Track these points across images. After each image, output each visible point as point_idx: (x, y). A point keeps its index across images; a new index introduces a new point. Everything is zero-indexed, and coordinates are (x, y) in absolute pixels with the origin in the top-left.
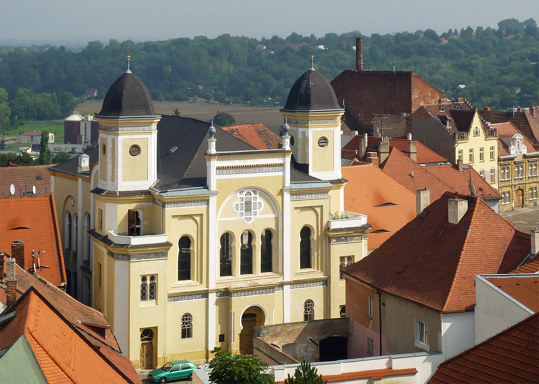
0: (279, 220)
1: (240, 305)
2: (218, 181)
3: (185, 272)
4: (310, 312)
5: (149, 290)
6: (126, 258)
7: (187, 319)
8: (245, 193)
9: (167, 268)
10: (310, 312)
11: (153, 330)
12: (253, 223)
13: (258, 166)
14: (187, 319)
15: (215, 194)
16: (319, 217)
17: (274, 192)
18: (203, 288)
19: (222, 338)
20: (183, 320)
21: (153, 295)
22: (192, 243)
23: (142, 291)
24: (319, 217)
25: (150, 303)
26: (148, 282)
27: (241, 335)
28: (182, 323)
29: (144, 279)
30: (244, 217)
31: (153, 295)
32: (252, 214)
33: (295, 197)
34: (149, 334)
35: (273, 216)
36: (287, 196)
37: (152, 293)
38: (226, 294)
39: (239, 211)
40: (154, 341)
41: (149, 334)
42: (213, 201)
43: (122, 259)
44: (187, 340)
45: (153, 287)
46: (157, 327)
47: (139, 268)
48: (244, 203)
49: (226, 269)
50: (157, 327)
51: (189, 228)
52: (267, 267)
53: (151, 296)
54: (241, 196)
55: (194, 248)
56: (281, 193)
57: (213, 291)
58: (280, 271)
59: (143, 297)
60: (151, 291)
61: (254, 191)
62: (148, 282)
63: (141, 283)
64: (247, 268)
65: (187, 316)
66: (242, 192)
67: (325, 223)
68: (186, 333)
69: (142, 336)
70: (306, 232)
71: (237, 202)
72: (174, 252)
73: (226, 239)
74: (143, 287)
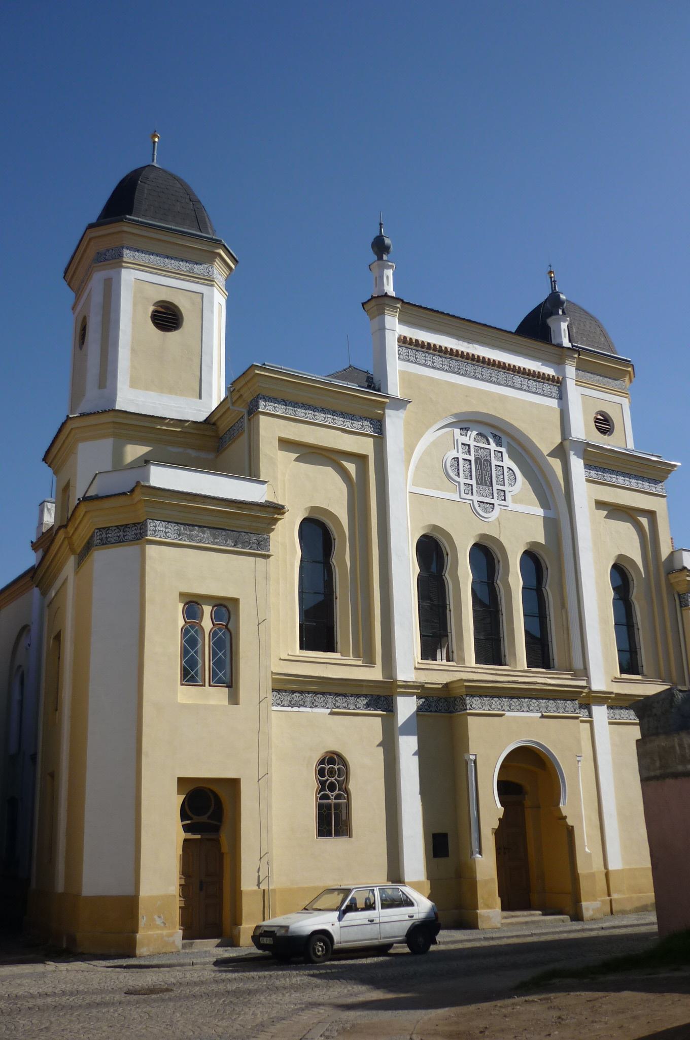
0: (559, 524)
1: (491, 741)
2: (402, 373)
3: (318, 632)
4: (338, 797)
5: (213, 652)
6: (130, 534)
7: (332, 771)
9: (269, 593)
10: (338, 797)
12: (498, 520)
14: (332, 771)
15: (400, 404)
16: (649, 542)
17: (545, 440)
18: (375, 674)
20: (321, 772)
22: (337, 544)
23: (185, 652)
24: (649, 542)
27: (498, 833)
28: (315, 785)
29: (192, 605)
30: (476, 498)
31: (226, 675)
32: (495, 495)
33: (593, 474)
34: (209, 808)
35: (540, 512)
36: (577, 465)
37: (218, 664)
38: (443, 709)
39: (472, 443)
40: (224, 837)
42: (394, 422)
43: (120, 541)
44: (333, 844)
46: (179, 779)
47: (174, 570)
49: (435, 636)
50: (179, 779)
51: (328, 492)
52: (540, 654)
53: (214, 674)
54: (465, 440)
55: (344, 558)
56: (561, 452)
57: (409, 689)
58: (578, 664)
60: (214, 654)
61: (495, 436)
63: (181, 622)
64: (491, 649)
65: (331, 761)
66: (467, 429)
67: (665, 552)
68: (332, 820)
69: (184, 815)
70: (621, 574)
71: (453, 454)
72: (286, 539)
73: (432, 550)
74: (190, 640)
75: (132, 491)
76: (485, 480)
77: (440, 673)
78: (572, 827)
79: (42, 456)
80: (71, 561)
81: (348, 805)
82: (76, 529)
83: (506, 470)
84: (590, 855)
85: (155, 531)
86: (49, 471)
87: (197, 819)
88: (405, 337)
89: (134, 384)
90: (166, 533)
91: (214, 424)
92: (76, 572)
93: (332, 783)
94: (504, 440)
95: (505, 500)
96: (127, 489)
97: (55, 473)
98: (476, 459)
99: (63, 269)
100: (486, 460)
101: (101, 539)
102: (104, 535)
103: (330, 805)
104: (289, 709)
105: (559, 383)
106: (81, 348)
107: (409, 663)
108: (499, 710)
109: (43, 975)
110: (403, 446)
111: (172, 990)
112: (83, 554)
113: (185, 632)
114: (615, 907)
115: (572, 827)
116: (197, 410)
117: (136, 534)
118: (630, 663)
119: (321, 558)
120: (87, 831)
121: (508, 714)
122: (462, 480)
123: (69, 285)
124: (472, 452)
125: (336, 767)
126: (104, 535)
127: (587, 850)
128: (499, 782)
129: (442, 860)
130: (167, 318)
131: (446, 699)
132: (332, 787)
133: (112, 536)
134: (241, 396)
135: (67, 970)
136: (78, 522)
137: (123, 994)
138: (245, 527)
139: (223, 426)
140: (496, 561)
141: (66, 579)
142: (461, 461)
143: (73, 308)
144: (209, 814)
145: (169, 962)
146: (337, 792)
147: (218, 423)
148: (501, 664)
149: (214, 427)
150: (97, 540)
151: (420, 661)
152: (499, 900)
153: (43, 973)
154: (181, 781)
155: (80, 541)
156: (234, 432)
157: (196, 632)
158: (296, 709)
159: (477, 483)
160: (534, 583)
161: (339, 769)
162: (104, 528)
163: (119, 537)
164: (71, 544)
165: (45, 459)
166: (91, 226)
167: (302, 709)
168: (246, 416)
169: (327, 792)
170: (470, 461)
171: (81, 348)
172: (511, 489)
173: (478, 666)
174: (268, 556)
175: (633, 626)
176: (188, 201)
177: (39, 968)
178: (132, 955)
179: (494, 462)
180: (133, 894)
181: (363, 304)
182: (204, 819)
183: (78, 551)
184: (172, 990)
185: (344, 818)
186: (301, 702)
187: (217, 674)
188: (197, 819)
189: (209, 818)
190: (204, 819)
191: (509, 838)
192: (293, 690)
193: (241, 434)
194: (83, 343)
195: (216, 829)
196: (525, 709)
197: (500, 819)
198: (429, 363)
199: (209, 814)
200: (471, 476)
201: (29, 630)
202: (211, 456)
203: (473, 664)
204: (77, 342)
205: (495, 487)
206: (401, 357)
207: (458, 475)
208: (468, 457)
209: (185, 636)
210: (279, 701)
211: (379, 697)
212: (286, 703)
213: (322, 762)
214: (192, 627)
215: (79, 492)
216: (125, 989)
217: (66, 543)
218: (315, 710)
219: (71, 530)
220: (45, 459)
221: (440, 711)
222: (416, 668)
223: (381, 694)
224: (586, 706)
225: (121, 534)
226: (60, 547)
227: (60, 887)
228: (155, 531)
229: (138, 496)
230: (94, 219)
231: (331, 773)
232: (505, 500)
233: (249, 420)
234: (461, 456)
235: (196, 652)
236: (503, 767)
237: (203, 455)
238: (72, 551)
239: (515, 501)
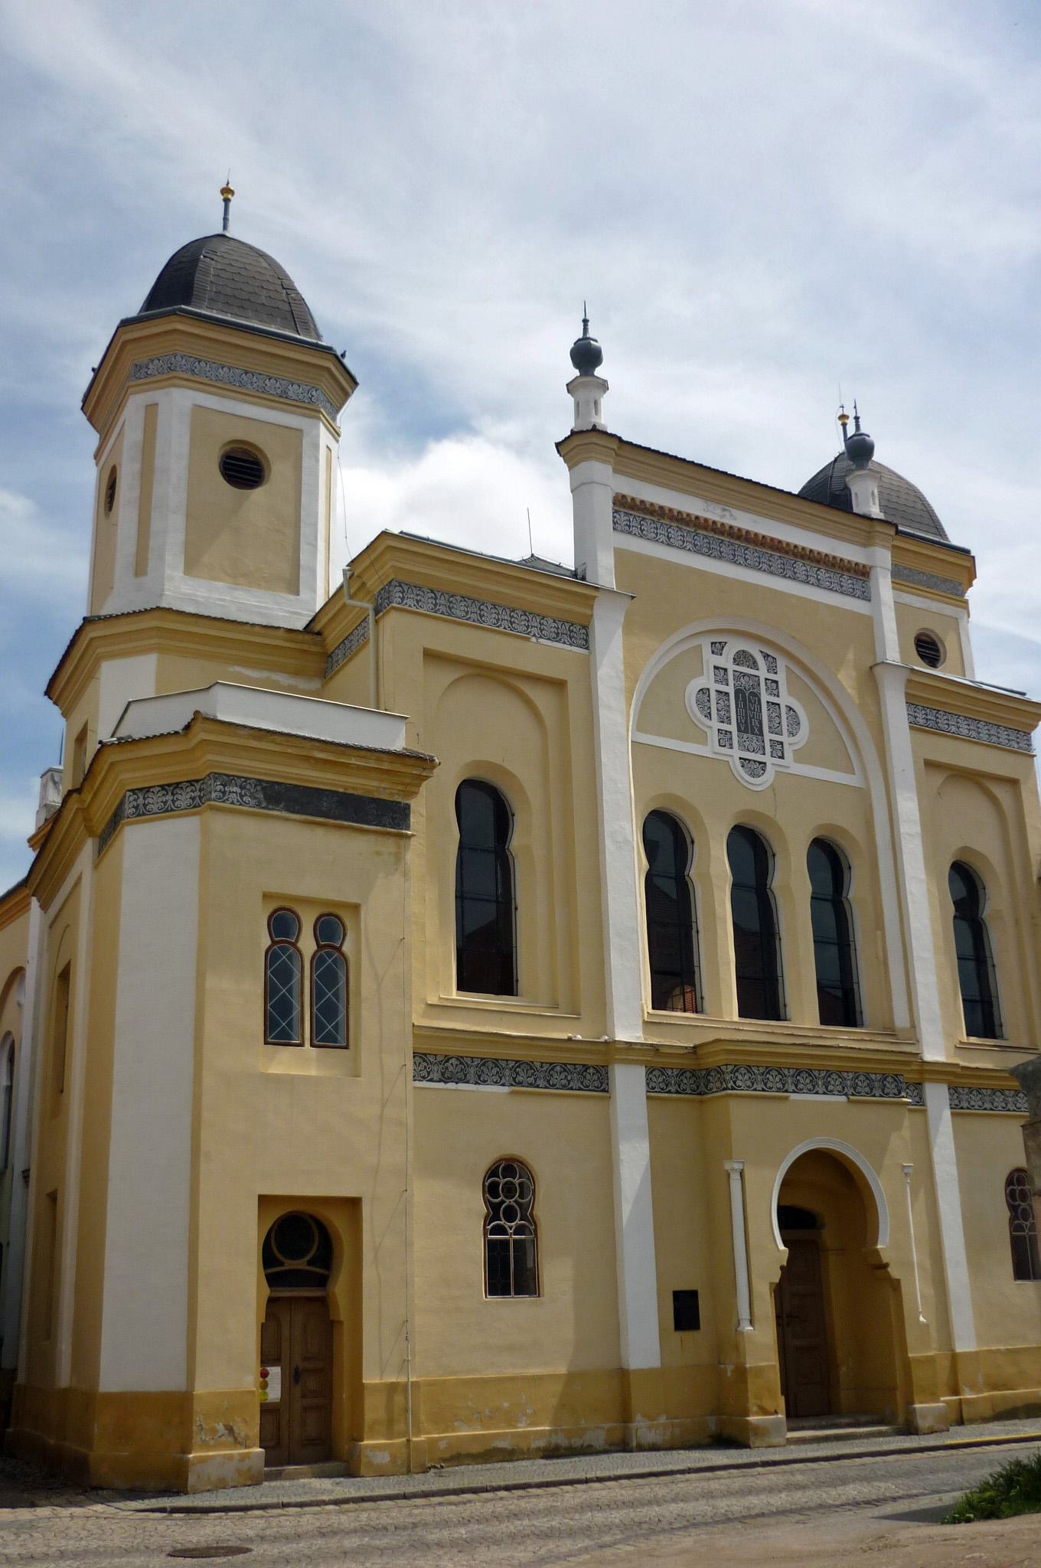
3: (487, 959)
4: (519, 1230)
5: (307, 988)
6: (184, 798)
8: (730, 651)
10: (519, 1230)
11: (338, 1222)
12: (772, 787)
13: (776, 546)
16: (1012, 826)
19: (685, 1310)
20: (491, 1190)
21: (331, 1030)
23: (270, 991)
25: (299, 1062)
26: (307, 944)
29: (282, 924)
31: (331, 1030)
32: (768, 749)
34: (305, 1248)
39: (731, 667)
40: (339, 1288)
41: (305, 1248)
43: (167, 811)
44: (514, 1308)
45: (332, 970)
46: (260, 1197)
48: (730, 689)
49: (674, 975)
50: (260, 1197)
52: (840, 1004)
55: (527, 841)
59: (278, 1028)
61: (766, 656)
62: (307, 944)
63: (266, 942)
64: (761, 994)
68: (510, 1270)
69: (268, 1258)
72: (434, 823)
73: (667, 838)
75: (187, 727)
76: (750, 725)
77: (682, 1030)
78: (899, 1281)
79: (44, 688)
80: (89, 847)
81: (535, 1243)
82: (95, 794)
83: (783, 710)
84: (927, 1326)
85: (224, 793)
86: (56, 711)
87: (290, 1265)
88: (624, 496)
89: (197, 408)
90: (242, 796)
91: (319, 633)
92: (96, 866)
93: (509, 1208)
94: (782, 663)
95: (782, 757)
96: (179, 728)
97: (65, 715)
98: (737, 692)
99: (81, 396)
100: (752, 694)
101: (136, 807)
102: (141, 801)
103: (507, 1242)
104: (441, 1085)
105: (862, 573)
106: (107, 516)
107: (630, 1013)
108: (779, 1090)
109: (31, 1526)
110: (622, 668)
111: (248, 1550)
112: (107, 835)
113: (271, 956)
114: (965, 1416)
115: (899, 1281)
116: (292, 612)
117: (193, 799)
118: (982, 1016)
119: (491, 843)
120: (108, 1275)
121: (793, 1096)
122: (715, 724)
123: (90, 419)
124: (731, 682)
125: (516, 1181)
126: (141, 801)
127: (922, 1319)
128: (780, 1208)
129: (688, 1336)
130: (243, 468)
131: (693, 1073)
132: (510, 1215)
133: (155, 801)
134: (364, 584)
135: (72, 1516)
136: (100, 779)
137: (163, 1556)
138: (362, 803)
139: (333, 638)
140: (769, 854)
141: (80, 878)
142: (713, 695)
143: (97, 456)
144: (308, 1258)
145: (242, 1503)
146: (518, 1222)
147: (326, 633)
148: (778, 1019)
149: (318, 638)
150: (129, 810)
151: (651, 1011)
152: (781, 1401)
153: (31, 1521)
154: (264, 1201)
155: (101, 815)
156: (351, 644)
157: (290, 957)
158: (451, 1086)
159: (739, 730)
160: (829, 890)
161: (521, 1184)
162: (141, 790)
163: (165, 803)
164: (87, 820)
165: (48, 693)
166: (125, 323)
167: (462, 1086)
168: (371, 613)
169: (502, 1222)
170: (727, 694)
171: (107, 516)
172: (792, 739)
173: (743, 1020)
174: (408, 837)
175: (985, 962)
176: (279, 288)
177: (24, 1514)
178: (180, 1490)
179: (765, 697)
180: (183, 1388)
181: (558, 445)
182: (301, 1264)
183: (99, 831)
184: (248, 1550)
185: (530, 1264)
186: (461, 1075)
187: (325, 1027)
188: (290, 1265)
189: (309, 1263)
190: (301, 1264)
191: (799, 1302)
192: (442, 1062)
193: (364, 646)
194: (110, 509)
195: (323, 1281)
196: (821, 1089)
197: (782, 1268)
198: (663, 538)
199: (308, 1258)
200: (729, 718)
201: (23, 976)
202: (315, 684)
203: (736, 1018)
204: (102, 504)
205: (768, 736)
206: (619, 527)
207: (709, 716)
208: (723, 688)
209: (272, 963)
210: (424, 1073)
211: (586, 1067)
212: (436, 1076)
213: (493, 1172)
214: (284, 950)
215: (103, 732)
216: (169, 1549)
217: (80, 816)
218: (482, 1088)
219: (87, 796)
220: (48, 693)
221: (684, 1092)
222: (645, 1023)
223: (589, 1063)
224: (917, 1088)
225: (169, 797)
226: (72, 822)
227: (64, 1377)
228: (224, 793)
229: (199, 734)
230: (133, 308)
231: (509, 1190)
232: (782, 757)
233: (377, 622)
234: (714, 687)
235: (290, 991)
236: (786, 1184)
237: (301, 683)
238: (90, 832)
239: (800, 757)
